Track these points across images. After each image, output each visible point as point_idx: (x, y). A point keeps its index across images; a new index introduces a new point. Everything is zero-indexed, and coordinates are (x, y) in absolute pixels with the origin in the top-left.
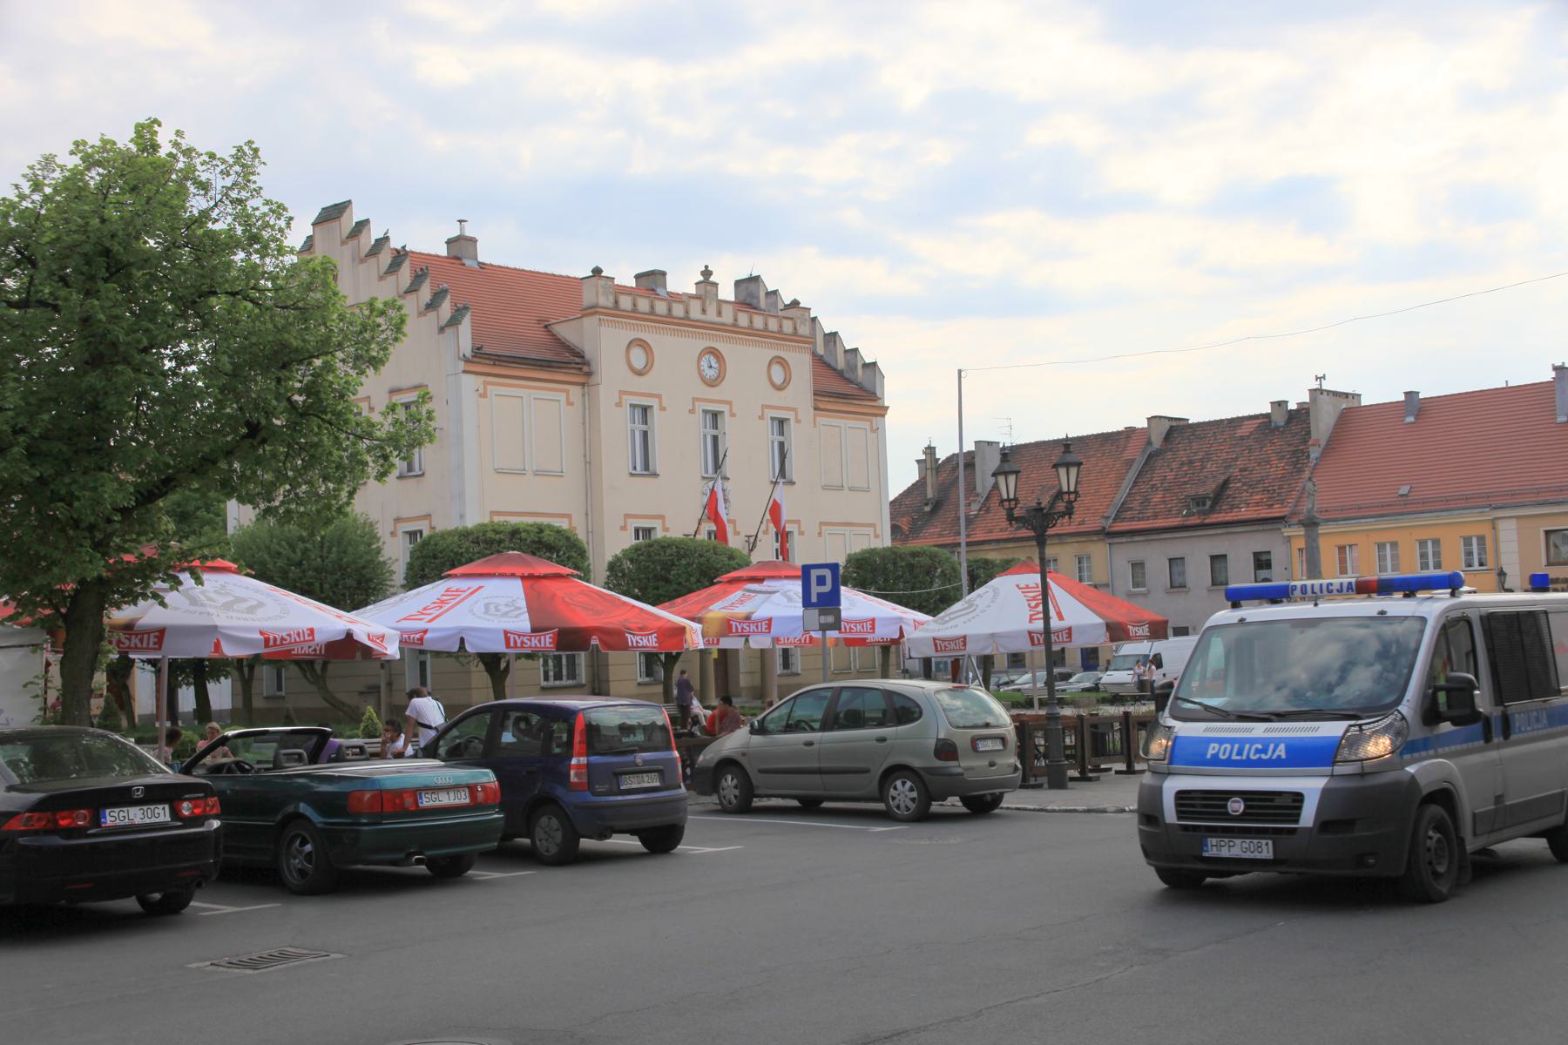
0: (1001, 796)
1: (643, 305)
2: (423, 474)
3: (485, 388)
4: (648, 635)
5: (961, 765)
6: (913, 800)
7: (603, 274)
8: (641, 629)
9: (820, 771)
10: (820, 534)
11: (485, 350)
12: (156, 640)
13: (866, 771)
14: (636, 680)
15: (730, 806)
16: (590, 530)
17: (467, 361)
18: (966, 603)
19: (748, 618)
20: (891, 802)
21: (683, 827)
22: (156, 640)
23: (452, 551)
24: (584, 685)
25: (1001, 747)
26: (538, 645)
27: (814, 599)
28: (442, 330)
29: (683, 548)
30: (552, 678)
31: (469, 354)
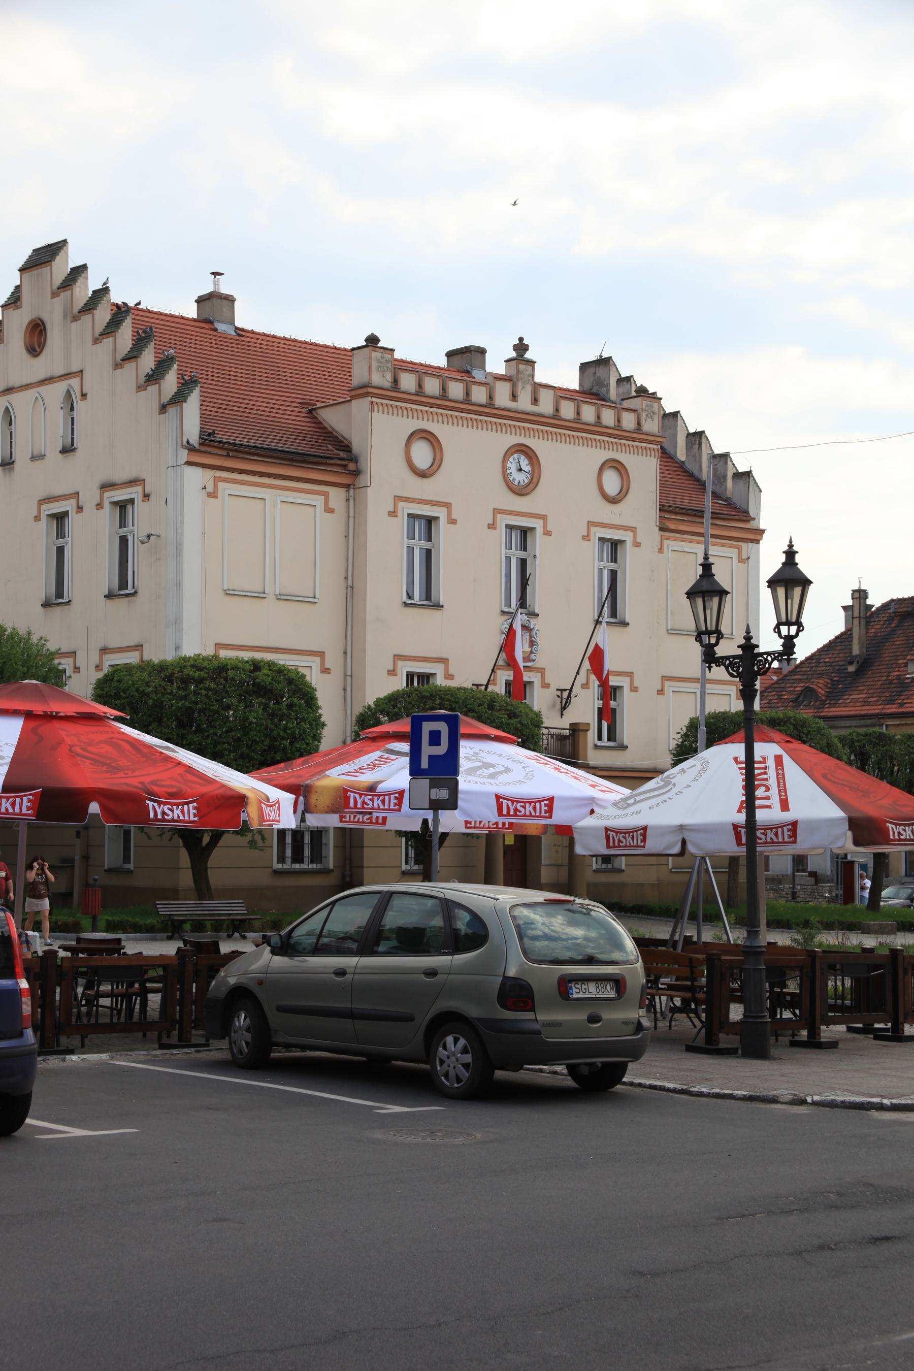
0: (621, 1069)
1: (456, 390)
2: (136, 592)
3: (215, 487)
4: (183, 804)
5: (539, 1018)
6: (466, 1066)
7: (380, 345)
8: (172, 795)
9: (350, 1015)
10: (661, 692)
11: (220, 437)
12: (396, 801)
13: (410, 1019)
14: (401, 867)
15: (240, 1057)
16: (349, 673)
17: (191, 449)
18: (662, 780)
19: (372, 788)
20: (439, 1068)
21: (28, 1097)
22: (396, 801)
23: (137, 690)
24: (332, 871)
25: (613, 994)
26: (11, 810)
27: (425, 764)
28: (163, 408)
29: (449, 700)
30: (289, 860)
31: (195, 440)
